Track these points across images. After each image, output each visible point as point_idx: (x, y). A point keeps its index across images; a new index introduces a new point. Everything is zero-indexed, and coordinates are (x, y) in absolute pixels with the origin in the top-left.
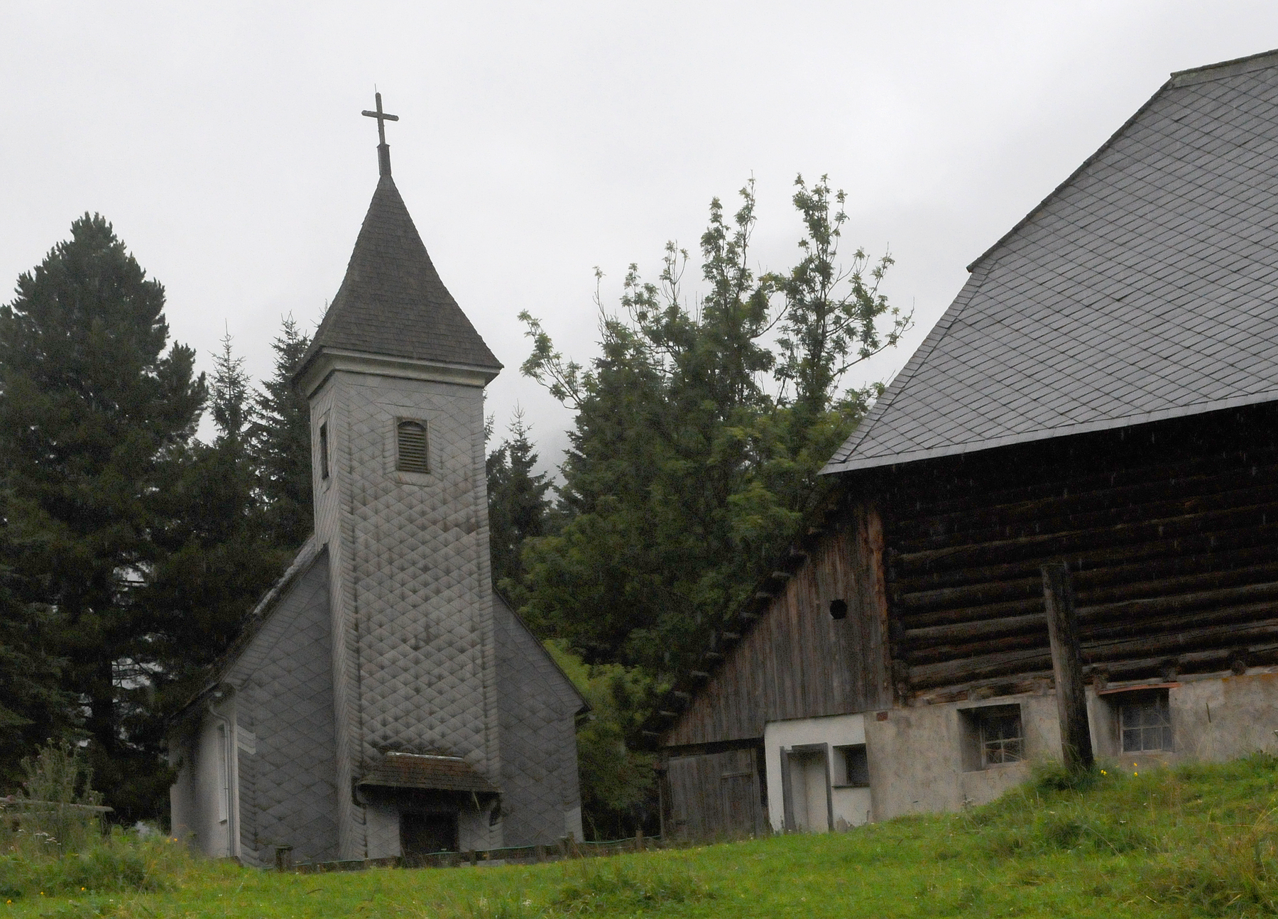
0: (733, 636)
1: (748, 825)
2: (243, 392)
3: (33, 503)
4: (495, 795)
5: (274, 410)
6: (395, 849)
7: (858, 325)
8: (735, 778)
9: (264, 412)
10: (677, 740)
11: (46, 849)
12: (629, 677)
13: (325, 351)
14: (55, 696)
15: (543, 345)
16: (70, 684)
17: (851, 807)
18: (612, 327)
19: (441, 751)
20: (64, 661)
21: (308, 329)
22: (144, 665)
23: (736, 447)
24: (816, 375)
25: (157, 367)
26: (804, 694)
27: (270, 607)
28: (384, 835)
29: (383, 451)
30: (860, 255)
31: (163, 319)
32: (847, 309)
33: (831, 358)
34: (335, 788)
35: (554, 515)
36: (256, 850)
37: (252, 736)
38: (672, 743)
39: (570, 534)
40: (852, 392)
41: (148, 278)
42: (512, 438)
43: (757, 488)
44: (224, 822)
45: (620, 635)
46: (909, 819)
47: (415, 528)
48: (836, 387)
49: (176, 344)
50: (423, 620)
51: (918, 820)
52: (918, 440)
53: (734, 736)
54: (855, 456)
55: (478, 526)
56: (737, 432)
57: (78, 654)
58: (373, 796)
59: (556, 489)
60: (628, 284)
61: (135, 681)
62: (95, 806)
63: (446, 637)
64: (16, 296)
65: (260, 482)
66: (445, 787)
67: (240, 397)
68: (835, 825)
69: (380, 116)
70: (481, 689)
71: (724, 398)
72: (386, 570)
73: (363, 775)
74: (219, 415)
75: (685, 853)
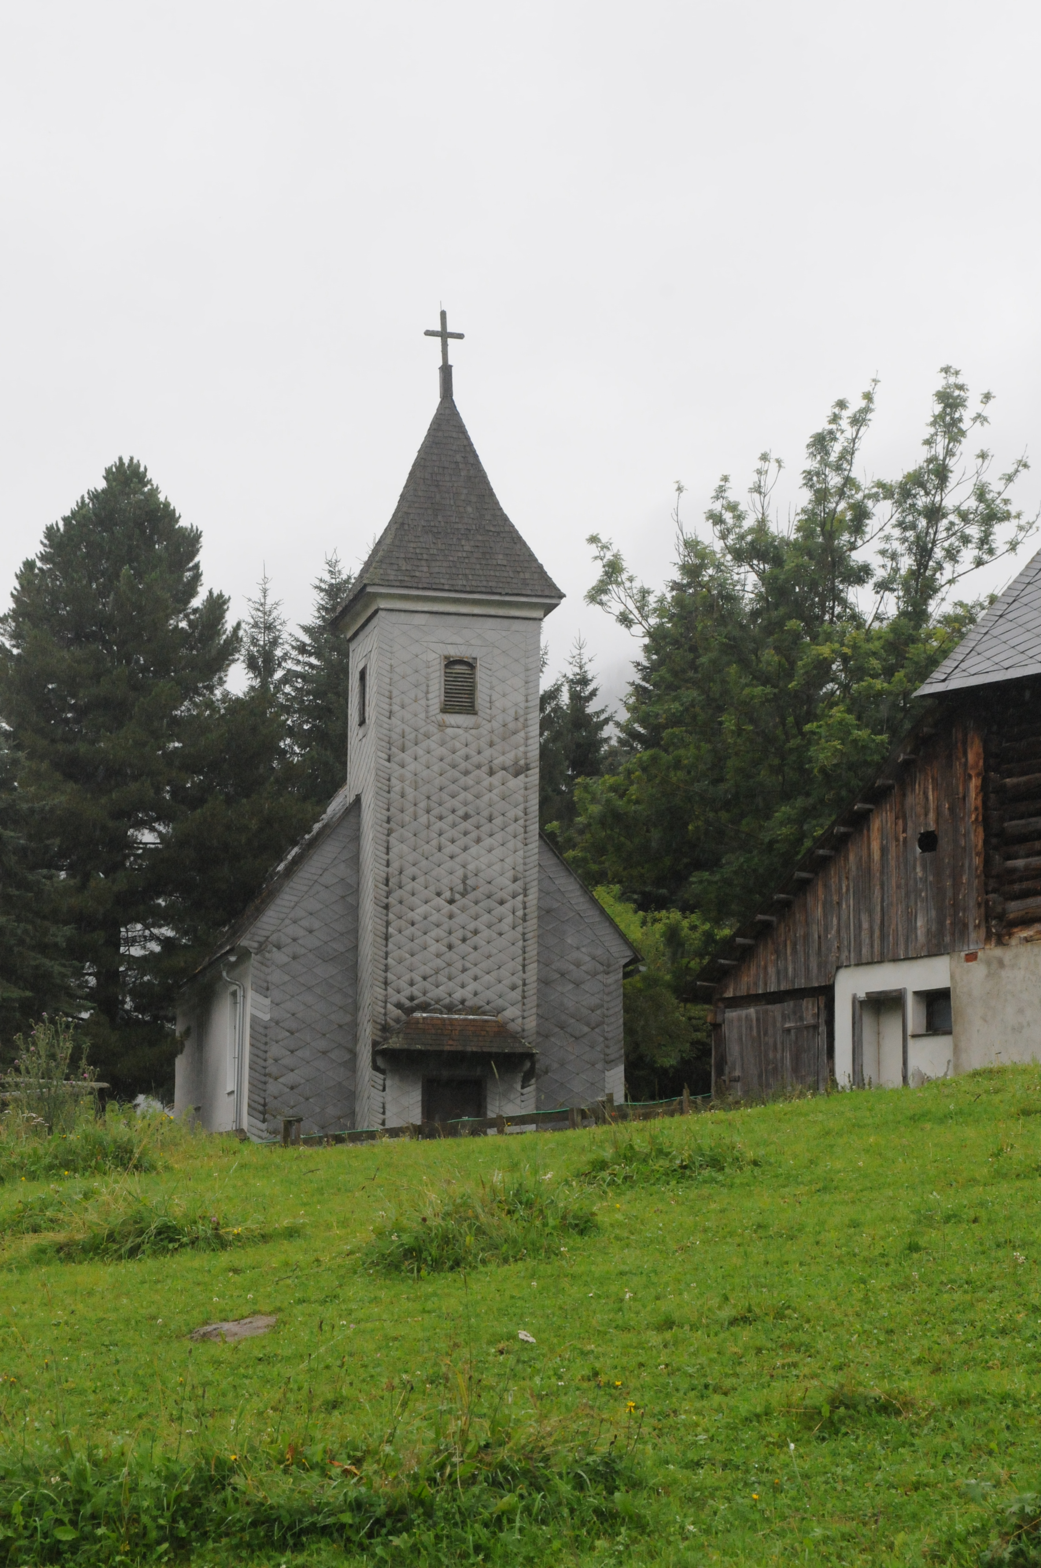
0: (804, 875)
1: (810, 1079)
2: (279, 637)
3: (44, 766)
4: (530, 1056)
5: (310, 654)
6: (416, 1117)
7: (974, 531)
8: (798, 1029)
9: (300, 658)
10: (734, 990)
11: (35, 1131)
12: (685, 923)
13: (369, 589)
14: (56, 967)
15: (613, 569)
16: (77, 952)
17: (930, 1057)
18: (691, 545)
19: (476, 1010)
20: (68, 930)
21: (352, 567)
22: (155, 931)
23: (822, 670)
24: (920, 587)
25: (187, 616)
26: (883, 937)
27: (297, 861)
28: (405, 1104)
29: (427, 693)
30: (983, 456)
31: (197, 566)
32: (964, 516)
33: (940, 567)
34: (354, 1054)
35: (613, 752)
36: (264, 1121)
37: (267, 1002)
38: (729, 994)
39: (629, 772)
40: (961, 604)
41: (183, 523)
42: (571, 671)
43: (837, 713)
44: (231, 1093)
45: (679, 878)
46: (991, 1071)
47: (457, 774)
48: (943, 599)
49: (211, 592)
50: (460, 872)
51: (1001, 1072)
52: (1030, 653)
53: (801, 983)
54: (958, 673)
55: (527, 768)
56: (825, 650)
57: (82, 920)
58: (393, 1061)
59: (618, 724)
60: (717, 498)
61: (144, 948)
62: (89, 1083)
63: (484, 889)
64: (41, 549)
65: (291, 732)
66: (475, 1049)
67: (275, 643)
68: (910, 1073)
69: (444, 335)
70: (521, 943)
71: (812, 621)
72: (423, 819)
73: (386, 1039)
74: (251, 664)
75: (732, 1115)
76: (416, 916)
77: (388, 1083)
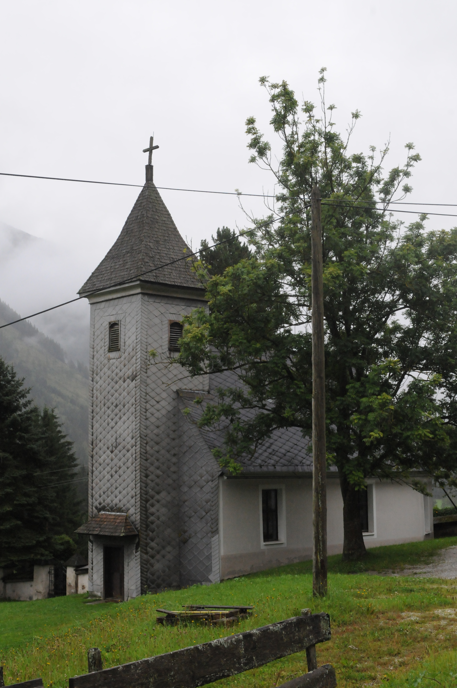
19: (119, 510)
30: (356, 116)
76: (101, 460)
77: (94, 548)
